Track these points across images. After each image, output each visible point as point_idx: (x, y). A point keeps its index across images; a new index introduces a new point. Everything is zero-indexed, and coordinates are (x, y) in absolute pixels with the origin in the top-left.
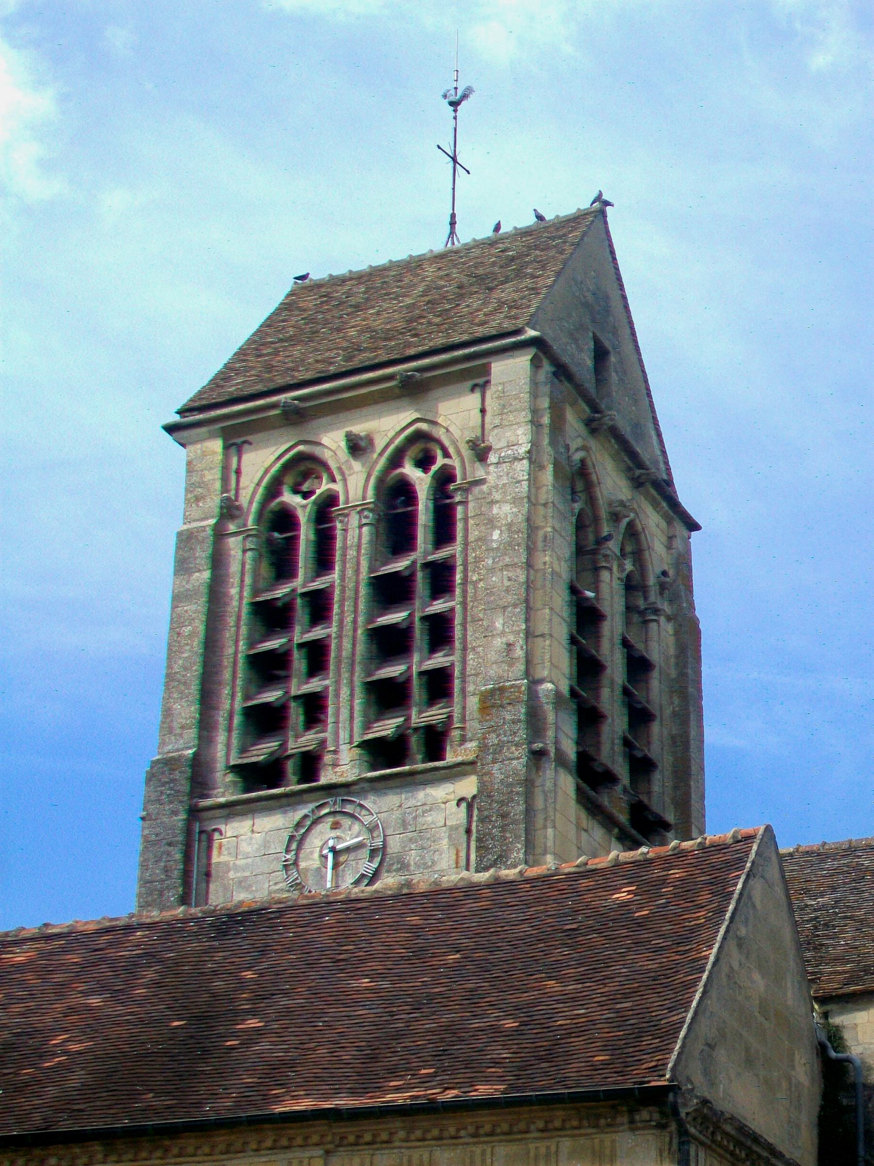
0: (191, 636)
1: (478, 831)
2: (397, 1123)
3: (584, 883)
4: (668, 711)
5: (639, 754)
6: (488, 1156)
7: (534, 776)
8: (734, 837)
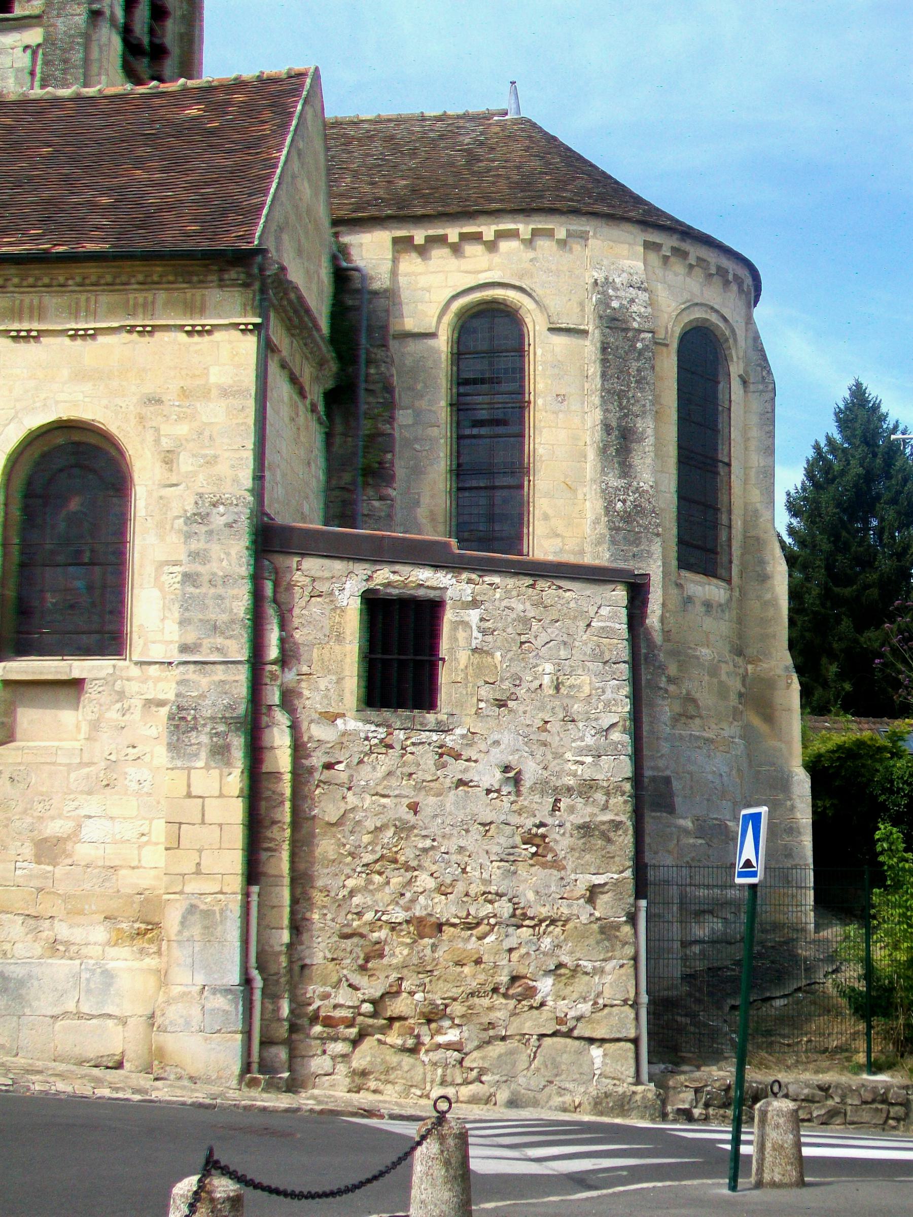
1: (42, 73)
2: (12, 270)
3: (157, 101)
4: (179, 13)
5: (157, 41)
6: (93, 302)
7: (91, 32)
8: (288, 73)
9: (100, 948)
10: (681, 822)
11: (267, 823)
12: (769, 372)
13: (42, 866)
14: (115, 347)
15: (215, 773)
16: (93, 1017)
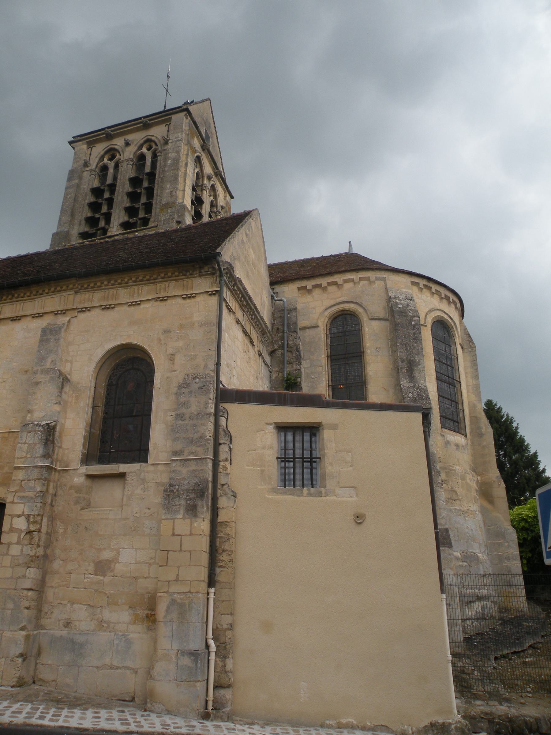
0: (70, 198)
9: (125, 625)
10: (455, 554)
11: (220, 551)
12: (473, 343)
13: (98, 577)
14: (149, 309)
15: (188, 521)
16: (117, 668)
